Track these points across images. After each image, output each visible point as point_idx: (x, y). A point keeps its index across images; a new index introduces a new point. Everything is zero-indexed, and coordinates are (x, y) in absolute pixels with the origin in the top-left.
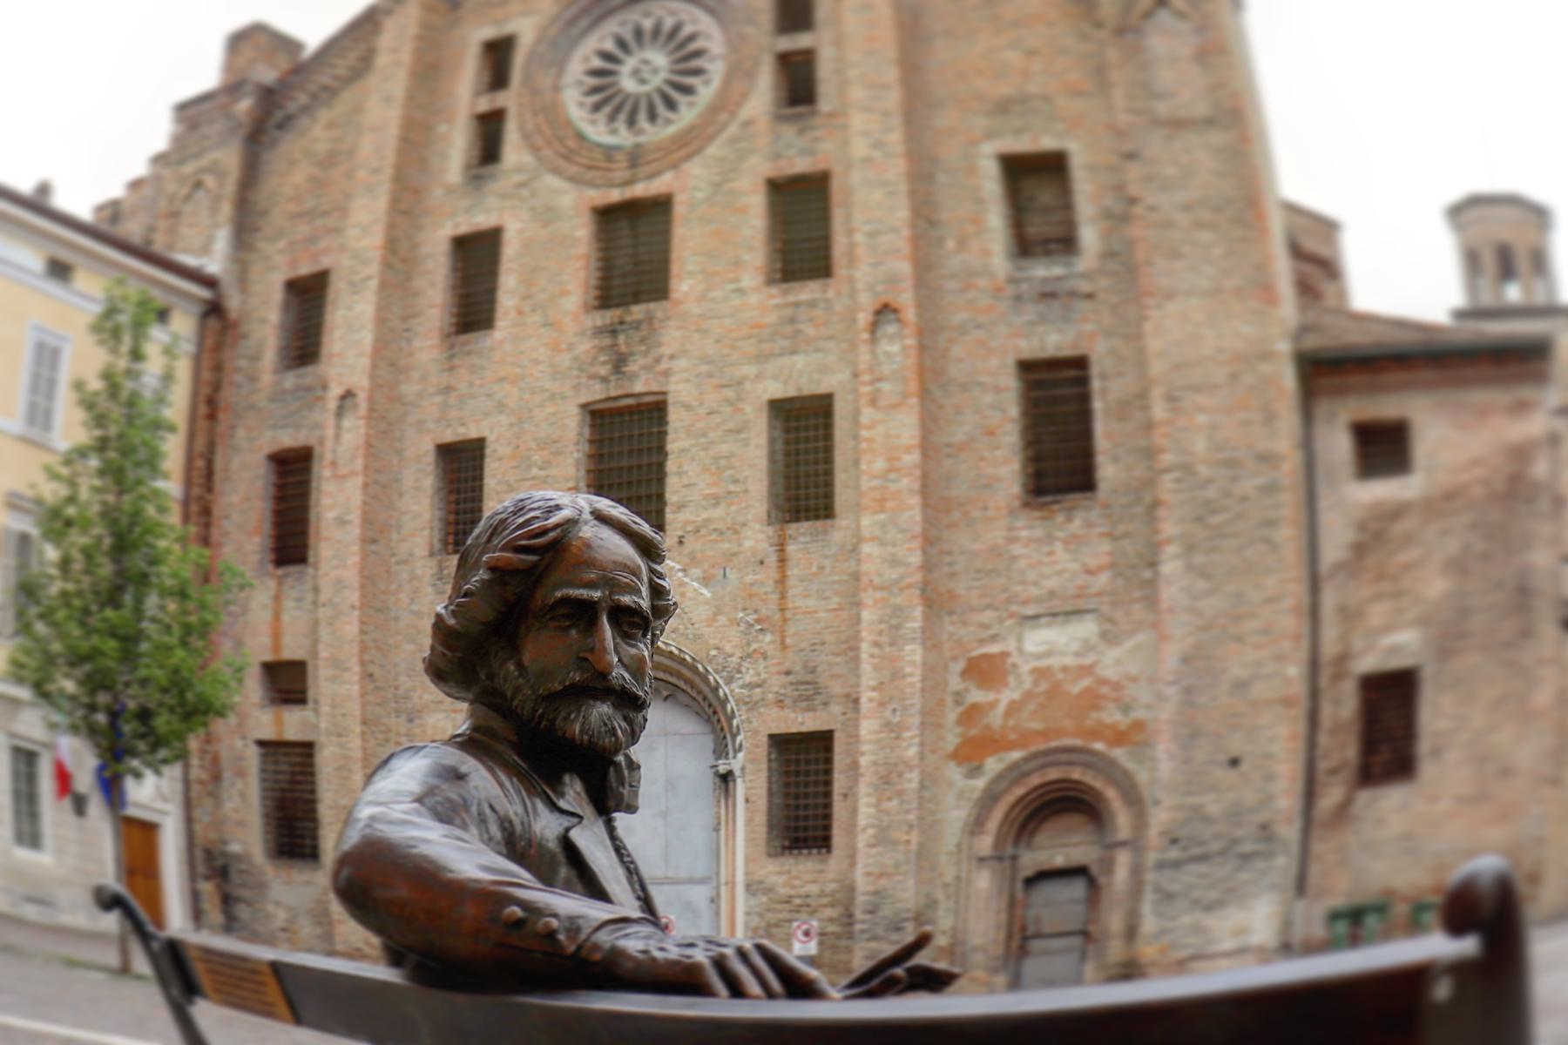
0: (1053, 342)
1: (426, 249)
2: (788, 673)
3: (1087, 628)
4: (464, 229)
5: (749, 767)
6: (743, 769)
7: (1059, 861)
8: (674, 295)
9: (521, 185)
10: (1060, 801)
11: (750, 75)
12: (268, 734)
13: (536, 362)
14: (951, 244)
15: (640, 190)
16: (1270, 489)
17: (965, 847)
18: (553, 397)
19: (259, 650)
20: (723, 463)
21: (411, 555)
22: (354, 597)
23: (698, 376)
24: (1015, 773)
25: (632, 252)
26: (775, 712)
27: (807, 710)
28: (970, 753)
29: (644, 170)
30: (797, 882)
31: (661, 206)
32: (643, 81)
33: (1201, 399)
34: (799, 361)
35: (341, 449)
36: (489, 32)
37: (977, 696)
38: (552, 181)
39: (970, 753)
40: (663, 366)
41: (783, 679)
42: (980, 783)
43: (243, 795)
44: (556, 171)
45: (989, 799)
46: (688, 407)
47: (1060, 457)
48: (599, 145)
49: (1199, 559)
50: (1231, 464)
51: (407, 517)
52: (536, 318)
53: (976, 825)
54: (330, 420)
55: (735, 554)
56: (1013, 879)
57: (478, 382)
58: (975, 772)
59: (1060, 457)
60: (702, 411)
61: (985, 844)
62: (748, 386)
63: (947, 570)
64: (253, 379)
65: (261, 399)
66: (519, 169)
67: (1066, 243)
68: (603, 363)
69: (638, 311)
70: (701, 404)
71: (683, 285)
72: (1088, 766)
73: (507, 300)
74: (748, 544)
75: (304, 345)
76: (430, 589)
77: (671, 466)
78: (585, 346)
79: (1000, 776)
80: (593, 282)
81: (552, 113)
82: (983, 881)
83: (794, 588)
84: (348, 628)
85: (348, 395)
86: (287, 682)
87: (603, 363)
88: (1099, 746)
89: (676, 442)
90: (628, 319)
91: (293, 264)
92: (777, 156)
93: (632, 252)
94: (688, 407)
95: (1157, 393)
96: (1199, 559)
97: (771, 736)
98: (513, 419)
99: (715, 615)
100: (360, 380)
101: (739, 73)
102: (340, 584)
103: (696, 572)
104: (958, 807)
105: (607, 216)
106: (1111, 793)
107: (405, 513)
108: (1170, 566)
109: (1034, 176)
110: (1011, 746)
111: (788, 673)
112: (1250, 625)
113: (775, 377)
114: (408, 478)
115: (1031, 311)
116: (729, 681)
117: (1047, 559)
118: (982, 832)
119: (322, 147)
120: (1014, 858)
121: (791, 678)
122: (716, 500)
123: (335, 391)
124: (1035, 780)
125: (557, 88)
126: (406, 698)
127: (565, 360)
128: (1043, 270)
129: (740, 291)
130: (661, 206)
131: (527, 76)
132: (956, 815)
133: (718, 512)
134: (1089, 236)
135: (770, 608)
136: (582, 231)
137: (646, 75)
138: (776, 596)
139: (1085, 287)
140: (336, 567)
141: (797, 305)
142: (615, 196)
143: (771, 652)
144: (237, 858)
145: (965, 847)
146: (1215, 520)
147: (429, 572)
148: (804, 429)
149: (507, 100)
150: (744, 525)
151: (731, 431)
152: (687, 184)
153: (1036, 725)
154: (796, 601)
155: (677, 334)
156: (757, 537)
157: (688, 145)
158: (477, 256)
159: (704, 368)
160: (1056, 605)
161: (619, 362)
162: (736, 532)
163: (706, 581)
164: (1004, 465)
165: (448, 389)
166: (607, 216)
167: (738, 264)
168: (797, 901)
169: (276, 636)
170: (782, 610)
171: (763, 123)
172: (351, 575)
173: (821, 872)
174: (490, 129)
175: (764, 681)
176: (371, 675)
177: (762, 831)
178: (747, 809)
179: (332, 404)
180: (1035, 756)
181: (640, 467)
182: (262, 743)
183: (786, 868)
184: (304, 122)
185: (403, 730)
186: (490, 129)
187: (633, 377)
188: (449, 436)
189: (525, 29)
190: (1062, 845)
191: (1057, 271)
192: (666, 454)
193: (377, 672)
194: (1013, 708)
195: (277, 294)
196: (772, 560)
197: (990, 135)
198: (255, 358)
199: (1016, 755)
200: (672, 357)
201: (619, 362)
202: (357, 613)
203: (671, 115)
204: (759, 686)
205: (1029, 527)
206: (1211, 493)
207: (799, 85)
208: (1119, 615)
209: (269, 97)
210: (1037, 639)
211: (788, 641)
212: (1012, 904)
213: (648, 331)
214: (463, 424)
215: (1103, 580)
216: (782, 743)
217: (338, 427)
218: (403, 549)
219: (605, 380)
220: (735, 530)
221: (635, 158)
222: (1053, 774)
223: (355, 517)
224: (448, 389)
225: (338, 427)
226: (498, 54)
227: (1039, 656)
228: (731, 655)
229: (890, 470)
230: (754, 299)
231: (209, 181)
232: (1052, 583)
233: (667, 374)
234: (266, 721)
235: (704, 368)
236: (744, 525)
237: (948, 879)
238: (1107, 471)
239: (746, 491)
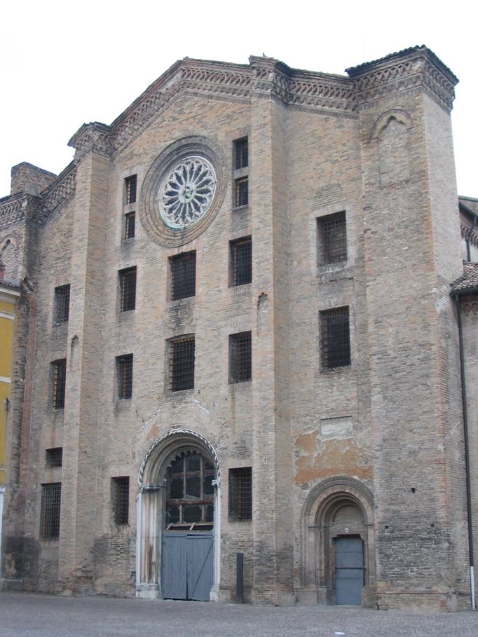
0: (334, 302)
1: (109, 276)
2: (235, 443)
3: (347, 425)
4: (122, 267)
5: (222, 483)
6: (220, 483)
7: (347, 531)
8: (197, 294)
9: (142, 247)
10: (340, 502)
11: (224, 192)
12: (46, 481)
13: (150, 323)
14: (295, 263)
15: (185, 249)
16: (427, 359)
17: (303, 521)
18: (156, 337)
19: (46, 444)
20: (214, 360)
21: (106, 401)
22: (77, 420)
23: (205, 326)
24: (321, 488)
25: (183, 272)
26: (231, 459)
27: (243, 459)
28: (302, 480)
29: (186, 240)
30: (240, 535)
31: (192, 254)
32: (187, 197)
33: (392, 321)
34: (239, 319)
35: (75, 359)
36: (127, 174)
37: (303, 453)
38: (153, 245)
39: (302, 480)
40: (194, 323)
41: (234, 446)
42: (307, 492)
43: (33, 510)
44: (155, 241)
45: (311, 499)
46: (202, 339)
47: (336, 351)
48: (172, 228)
49: (390, 393)
50: (404, 349)
51: (105, 386)
52: (149, 305)
53: (307, 511)
54: (69, 348)
55: (217, 396)
56: (326, 537)
57: (130, 331)
58: (305, 486)
59: (336, 351)
60: (207, 341)
61: (312, 520)
62: (222, 329)
63: (292, 400)
64: (44, 330)
65: (47, 339)
66: (141, 241)
67: (343, 257)
68: (173, 323)
69: (185, 300)
70: (206, 338)
71: (200, 289)
72: (352, 486)
73: (139, 297)
74: (221, 392)
75: (63, 313)
76: (112, 415)
77: (196, 363)
78: (167, 316)
79: (315, 490)
80: (171, 289)
81: (153, 214)
82: (312, 538)
83: (237, 409)
84: (75, 433)
85: (75, 338)
86: (55, 456)
87: (173, 323)
88: (356, 477)
89: (198, 353)
90: (181, 304)
91: (57, 281)
92: (233, 230)
93: (183, 272)
94: (202, 339)
95: (371, 320)
96: (390, 393)
97: (230, 470)
98: (142, 346)
99: (211, 421)
100: (80, 332)
101: (221, 191)
102: (72, 416)
103: (204, 404)
104: (299, 502)
105: (174, 260)
106: (363, 500)
107: (104, 385)
108: (376, 398)
109: (332, 226)
110: (319, 476)
111: (235, 443)
112: (415, 424)
113: (231, 326)
114: (105, 371)
115: (325, 289)
116: (215, 447)
117: (330, 395)
118: (309, 514)
119: (65, 227)
120: (326, 528)
121: (236, 446)
122: (211, 375)
123: (71, 336)
124: (330, 491)
125: (155, 202)
126: (103, 460)
127: (160, 322)
128: (331, 270)
129: (219, 291)
130: (192, 254)
131: (142, 196)
132: (298, 505)
133: (211, 380)
134: (352, 251)
135: (228, 417)
136: (165, 267)
137: (188, 195)
138: (231, 413)
139: (349, 275)
140: (71, 408)
141: (239, 295)
142: (176, 252)
143: (230, 434)
144: (28, 539)
145: (303, 521)
146: (397, 375)
147: (112, 407)
148: (241, 343)
149: (136, 207)
150: (220, 384)
151: (216, 348)
152: (199, 245)
153: (329, 467)
154: (238, 415)
155: (198, 310)
156: (225, 390)
157: (202, 228)
158: (128, 276)
159: (207, 323)
160: (334, 414)
161: (178, 322)
162: (218, 388)
163: (207, 408)
164: (313, 356)
165: (119, 335)
166: (174, 260)
167: (219, 279)
168: (240, 544)
169: (53, 438)
170: (234, 418)
171: (228, 214)
172: (76, 411)
173: (248, 530)
174: (130, 217)
175: (228, 447)
176: (85, 452)
177: (227, 511)
178: (221, 501)
179: (69, 342)
180: (329, 480)
181: (187, 363)
182: (43, 485)
183: (236, 528)
184: (56, 214)
185: (100, 474)
186: (130, 217)
187: (183, 328)
188: (120, 354)
189: (141, 172)
190: (346, 525)
191: (337, 269)
192: (194, 358)
193: (88, 450)
194: (319, 459)
195: (52, 294)
196: (230, 398)
197: (314, 209)
198: (44, 321)
199: (319, 480)
200: (196, 319)
201: (178, 322)
202: (78, 427)
203: (197, 213)
204: (226, 449)
205: (323, 381)
206: (396, 363)
207: (242, 191)
208: (361, 419)
209: (38, 202)
210: (327, 429)
211: (236, 431)
212: (327, 552)
213: (188, 310)
214: (125, 348)
215: (354, 403)
216: (233, 472)
217: (72, 351)
218: (103, 399)
219: (174, 329)
220: (217, 387)
221: (184, 233)
222: (337, 489)
223: (79, 387)
224: (119, 335)
225: (72, 351)
226: (131, 181)
227: (328, 436)
228: (216, 437)
229: (263, 361)
230: (224, 294)
231: (12, 240)
232: (332, 405)
233: (195, 326)
234: (47, 476)
235: (207, 323)
236: (220, 384)
237: (297, 535)
238: (355, 355)
239: (221, 371)
